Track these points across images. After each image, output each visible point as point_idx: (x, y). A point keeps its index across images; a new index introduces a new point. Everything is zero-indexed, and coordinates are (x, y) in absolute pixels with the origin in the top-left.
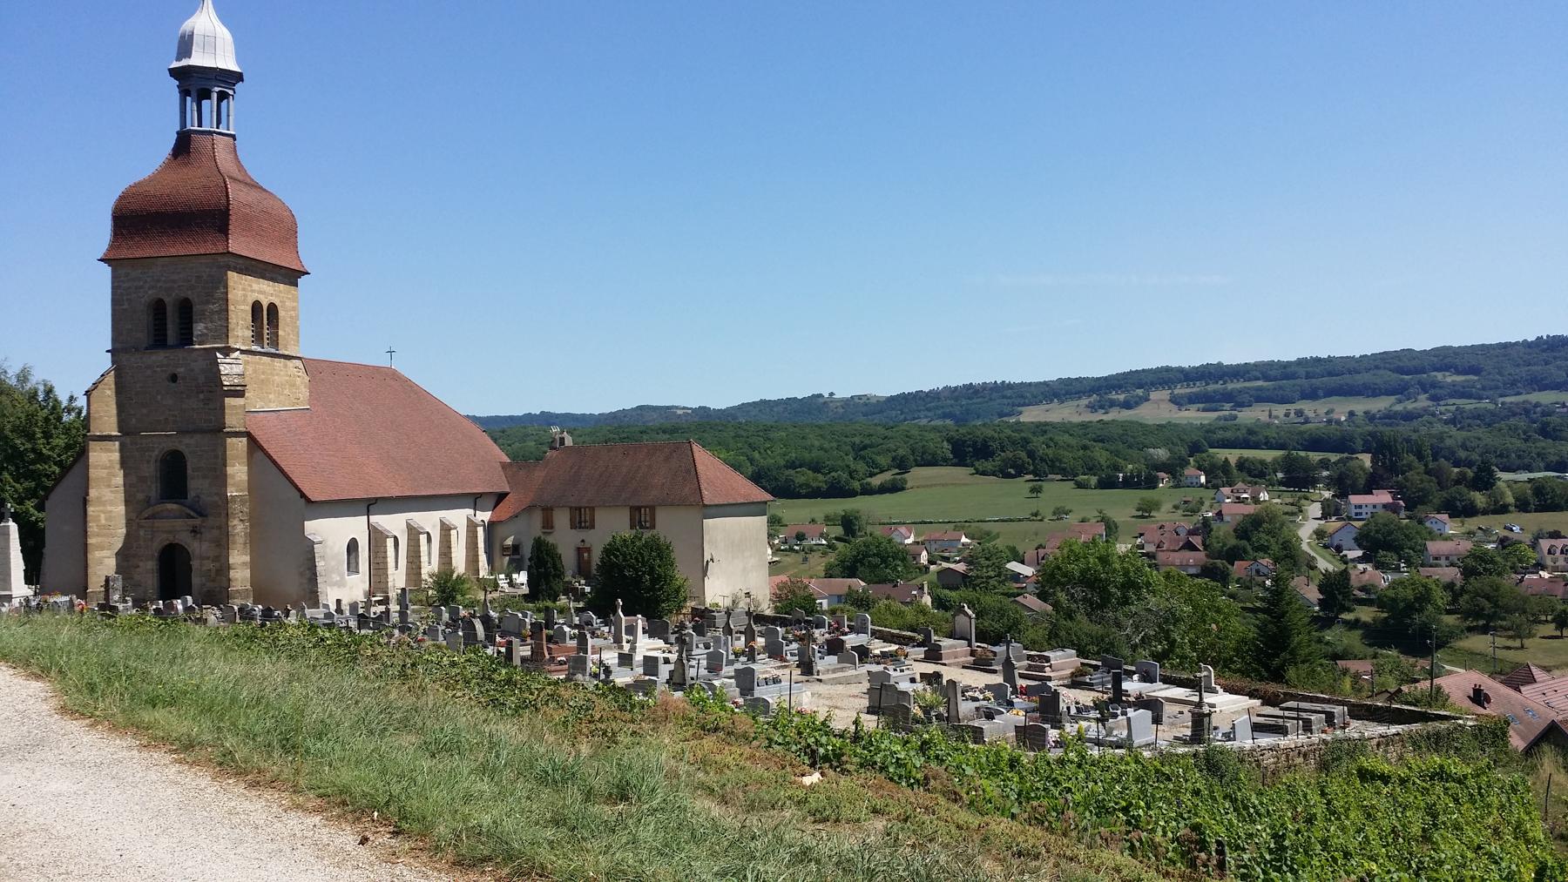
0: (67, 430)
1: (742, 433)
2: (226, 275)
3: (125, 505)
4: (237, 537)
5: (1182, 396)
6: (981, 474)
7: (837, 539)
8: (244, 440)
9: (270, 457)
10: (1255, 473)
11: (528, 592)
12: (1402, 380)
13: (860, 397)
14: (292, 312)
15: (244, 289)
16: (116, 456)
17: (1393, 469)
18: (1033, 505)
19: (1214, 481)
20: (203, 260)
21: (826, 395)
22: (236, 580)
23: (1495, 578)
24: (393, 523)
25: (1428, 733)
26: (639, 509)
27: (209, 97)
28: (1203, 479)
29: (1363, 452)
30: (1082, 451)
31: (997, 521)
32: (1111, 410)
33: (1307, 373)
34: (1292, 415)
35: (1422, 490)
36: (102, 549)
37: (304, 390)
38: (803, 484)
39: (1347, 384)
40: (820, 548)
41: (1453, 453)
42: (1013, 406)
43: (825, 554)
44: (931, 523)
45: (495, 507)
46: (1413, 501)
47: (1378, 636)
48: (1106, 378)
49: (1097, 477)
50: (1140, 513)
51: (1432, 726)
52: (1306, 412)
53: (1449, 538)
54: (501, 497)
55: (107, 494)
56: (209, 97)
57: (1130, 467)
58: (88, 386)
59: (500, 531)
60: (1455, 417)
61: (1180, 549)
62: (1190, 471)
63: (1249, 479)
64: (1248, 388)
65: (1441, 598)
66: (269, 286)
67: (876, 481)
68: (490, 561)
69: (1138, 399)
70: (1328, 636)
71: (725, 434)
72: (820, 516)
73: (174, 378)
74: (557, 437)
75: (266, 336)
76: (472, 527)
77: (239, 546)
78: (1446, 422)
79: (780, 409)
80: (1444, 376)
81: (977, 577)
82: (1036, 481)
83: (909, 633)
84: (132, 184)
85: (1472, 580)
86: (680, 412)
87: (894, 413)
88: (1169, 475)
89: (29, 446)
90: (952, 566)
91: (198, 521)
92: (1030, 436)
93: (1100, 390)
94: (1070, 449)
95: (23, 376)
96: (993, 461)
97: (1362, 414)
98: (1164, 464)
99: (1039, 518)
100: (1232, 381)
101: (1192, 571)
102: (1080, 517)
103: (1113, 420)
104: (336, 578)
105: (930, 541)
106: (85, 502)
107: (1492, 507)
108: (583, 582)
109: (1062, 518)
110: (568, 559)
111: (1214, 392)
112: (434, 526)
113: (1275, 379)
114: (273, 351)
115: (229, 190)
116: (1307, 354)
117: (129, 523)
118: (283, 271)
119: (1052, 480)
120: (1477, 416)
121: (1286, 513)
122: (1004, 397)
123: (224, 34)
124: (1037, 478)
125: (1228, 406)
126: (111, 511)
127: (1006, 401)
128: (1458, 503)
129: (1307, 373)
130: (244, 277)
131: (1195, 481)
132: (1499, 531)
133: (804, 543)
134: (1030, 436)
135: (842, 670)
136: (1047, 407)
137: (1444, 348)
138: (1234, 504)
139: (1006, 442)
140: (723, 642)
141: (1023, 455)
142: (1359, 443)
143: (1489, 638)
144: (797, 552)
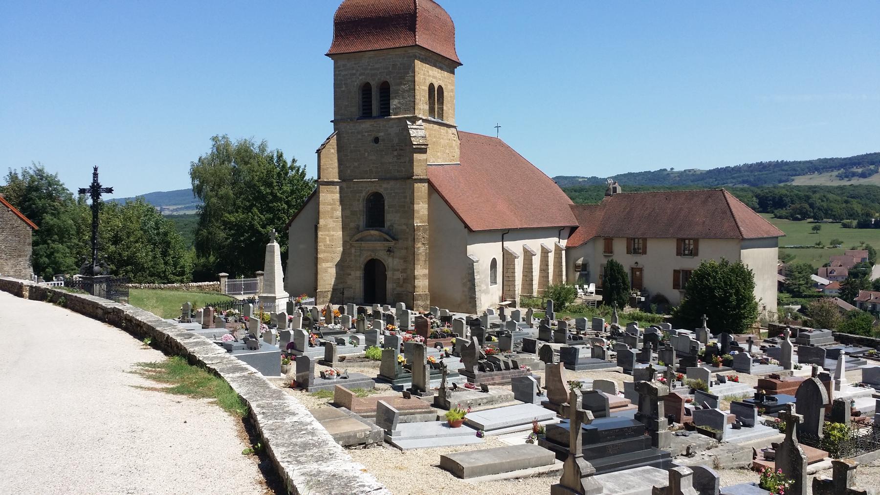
2: (414, 62)
3: (343, 232)
4: (420, 257)
6: (778, 218)
8: (426, 185)
13: (689, 171)
14: (451, 93)
15: (424, 74)
16: (337, 196)
18: (816, 238)
20: (398, 52)
21: (669, 170)
22: (419, 287)
24: (516, 247)
26: (684, 240)
31: (793, 248)
32: (853, 178)
42: (788, 176)
48: (850, 159)
49: (857, 221)
54: (573, 229)
58: (318, 146)
59: (574, 253)
66: (435, 71)
69: (870, 172)
73: (376, 140)
74: (611, 187)
77: (421, 263)
82: (816, 222)
86: (580, 180)
87: (711, 180)
89: (268, 191)
91: (392, 244)
92: (811, 194)
93: (845, 166)
94: (836, 202)
95: (263, 148)
96: (786, 209)
99: (821, 246)
102: (851, 246)
103: (860, 185)
106: (316, 228)
108: (639, 293)
109: (836, 247)
112: (538, 250)
114: (440, 121)
122: (783, 170)
124: (816, 221)
126: (333, 235)
127: (784, 173)
134: (811, 194)
136: (811, 176)
139: (795, 198)
141: (807, 206)
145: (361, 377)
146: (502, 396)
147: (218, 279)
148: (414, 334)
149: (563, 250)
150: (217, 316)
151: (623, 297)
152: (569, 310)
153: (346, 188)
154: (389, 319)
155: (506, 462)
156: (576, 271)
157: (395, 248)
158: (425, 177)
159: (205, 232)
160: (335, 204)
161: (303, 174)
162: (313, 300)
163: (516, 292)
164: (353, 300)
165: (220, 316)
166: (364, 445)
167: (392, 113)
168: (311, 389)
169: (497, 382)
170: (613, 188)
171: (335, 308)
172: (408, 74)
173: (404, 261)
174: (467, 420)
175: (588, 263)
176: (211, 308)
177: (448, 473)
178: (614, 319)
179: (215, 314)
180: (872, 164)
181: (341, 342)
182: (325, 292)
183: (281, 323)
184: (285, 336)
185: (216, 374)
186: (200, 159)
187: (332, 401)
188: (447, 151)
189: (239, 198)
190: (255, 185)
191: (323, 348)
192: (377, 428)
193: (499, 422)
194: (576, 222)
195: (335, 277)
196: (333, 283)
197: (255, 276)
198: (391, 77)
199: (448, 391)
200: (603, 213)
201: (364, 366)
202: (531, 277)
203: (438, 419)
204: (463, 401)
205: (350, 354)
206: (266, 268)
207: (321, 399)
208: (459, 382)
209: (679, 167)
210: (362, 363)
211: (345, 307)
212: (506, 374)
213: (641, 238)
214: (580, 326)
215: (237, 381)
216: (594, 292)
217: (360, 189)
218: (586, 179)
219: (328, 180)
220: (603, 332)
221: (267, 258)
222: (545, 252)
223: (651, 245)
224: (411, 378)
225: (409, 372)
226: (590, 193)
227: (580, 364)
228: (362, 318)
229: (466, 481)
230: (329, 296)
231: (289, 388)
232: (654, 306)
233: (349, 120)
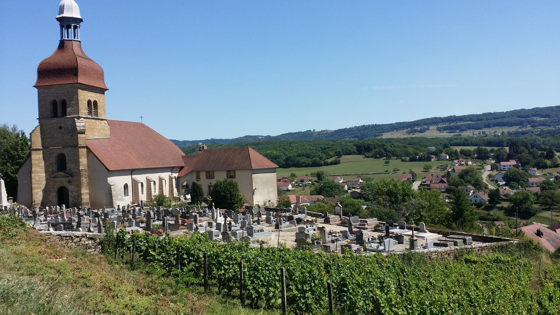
1: (281, 144)
2: (77, 91)
3: (45, 173)
4: (84, 184)
5: (441, 128)
7: (315, 181)
8: (86, 149)
9: (95, 155)
10: (467, 155)
11: (190, 202)
12: (521, 120)
13: (324, 131)
15: (84, 96)
16: (41, 156)
17: (517, 152)
18: (386, 168)
19: (452, 158)
20: (70, 86)
21: (312, 130)
22: (84, 199)
23: (552, 191)
24: (141, 178)
25: (498, 245)
27: (70, 28)
28: (448, 157)
29: (507, 146)
30: (404, 148)
33: (487, 118)
34: (481, 134)
35: (527, 159)
37: (108, 131)
38: (304, 162)
39: (501, 122)
40: (309, 185)
41: (539, 146)
43: (311, 187)
44: (349, 175)
46: (524, 164)
47: (509, 212)
48: (413, 122)
50: (425, 170)
51: (500, 243)
52: (486, 133)
53: (537, 177)
54: (182, 168)
55: (38, 169)
56: (70, 28)
57: (421, 153)
58: (31, 131)
59: (181, 180)
60: (540, 133)
61: (439, 183)
62: (443, 154)
63: (465, 157)
64: (465, 124)
65: (532, 198)
67: (329, 161)
68: (178, 191)
70: (492, 213)
71: (276, 145)
72: (309, 173)
73: (61, 128)
75: (93, 112)
76: (171, 179)
78: (537, 135)
79: (296, 135)
80: (537, 118)
81: (365, 194)
83: (320, 213)
85: (544, 191)
86: (260, 138)
88: (436, 156)
89: (16, 153)
90: (356, 190)
91: (70, 178)
95: (14, 129)
96: (372, 152)
97: (506, 133)
98: (434, 152)
99: (388, 172)
100: (459, 122)
101: (443, 190)
102: (403, 172)
104: (120, 197)
105: (348, 181)
106: (31, 172)
107: (553, 165)
109: (396, 173)
110: (205, 190)
111: (453, 126)
112: (157, 179)
113: (475, 121)
114: (96, 117)
116: (486, 111)
117: (47, 179)
118: (99, 89)
119: (393, 159)
120: (549, 132)
121: (478, 169)
122: (376, 130)
125: (458, 131)
127: (377, 131)
128: (540, 164)
129: (487, 118)
130: (84, 91)
131: (445, 158)
132: (555, 174)
133: (304, 183)
135: (290, 227)
136: (392, 133)
137: (536, 108)
138: (458, 166)
140: (249, 218)
141: (382, 150)
142: (505, 144)
143: (550, 212)
144: (301, 186)
157: (73, 180)
160: (41, 160)
180: (426, 125)
209: (318, 129)
218: (264, 137)
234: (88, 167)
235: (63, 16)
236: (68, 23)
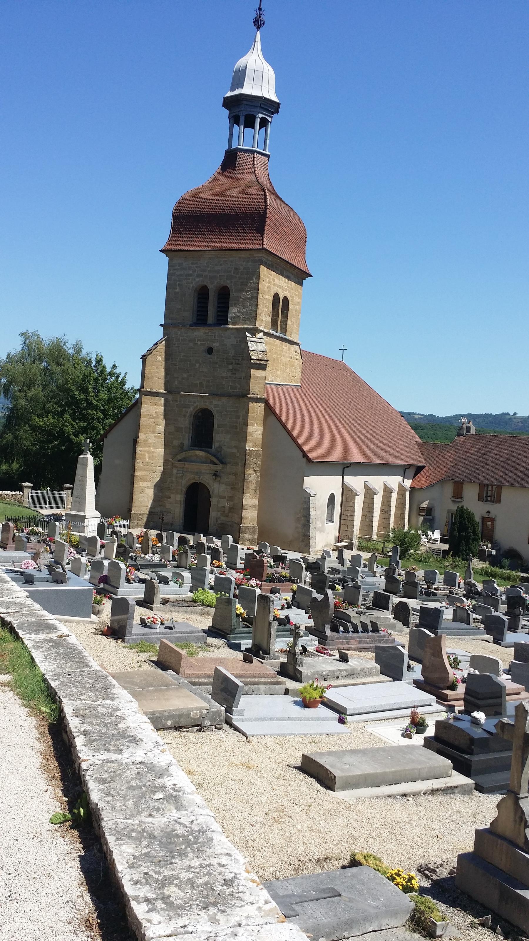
0: (109, 389)
4: (250, 484)
8: (263, 405)
9: (280, 421)
14: (297, 307)
15: (269, 282)
16: (161, 409)
20: (243, 255)
21: (512, 414)
22: (247, 518)
36: (145, 481)
45: (414, 478)
54: (419, 469)
58: (144, 352)
59: (418, 495)
66: (282, 280)
73: (210, 351)
74: (465, 426)
77: (251, 492)
84: (189, 191)
86: (416, 417)
89: (83, 396)
91: (219, 467)
106: (135, 443)
108: (489, 546)
112: (380, 488)
114: (283, 336)
115: (268, 197)
117: (166, 462)
123: (269, 72)
145: (190, 629)
146: (366, 669)
147: (21, 489)
148: (245, 575)
149: (407, 490)
150: (18, 534)
151: (473, 548)
152: (414, 559)
153: (173, 401)
154: (215, 554)
155: (390, 772)
156: (419, 515)
158: (262, 397)
159: (9, 436)
161: (123, 382)
162: (127, 523)
163: (355, 533)
164: (171, 528)
165: (20, 534)
166: (199, 727)
167: (230, 322)
168: (129, 639)
169: (353, 646)
170: (467, 427)
171: (153, 533)
172: (252, 279)
173: (231, 488)
174: (326, 699)
175: (434, 507)
176: (11, 524)
177: (313, 781)
178: (468, 573)
179: (15, 531)
181: (164, 580)
182: (140, 514)
183: (90, 548)
184: (97, 566)
185: (12, 631)
186: (8, 355)
187: (155, 659)
188: (288, 370)
189: (50, 402)
190: (69, 389)
191: (143, 586)
192: (217, 706)
193: (367, 705)
194: (424, 461)
195: (152, 498)
196: (149, 506)
197: (62, 489)
198: (231, 282)
199: (299, 657)
200: (454, 454)
201: (191, 613)
202: (371, 518)
203: (286, 692)
204: (318, 671)
205: (174, 596)
206: (77, 482)
207: (140, 654)
208: (308, 643)
210: (190, 609)
211: (164, 534)
212: (364, 637)
213: (495, 485)
214: (430, 578)
215: (42, 648)
216: (439, 540)
217: (188, 403)
218: (422, 417)
219: (152, 391)
220: (457, 588)
221: (79, 471)
222: (388, 491)
223: (506, 494)
224: (251, 635)
225: (248, 627)
226: (426, 431)
227: (443, 629)
228: (185, 551)
229: (339, 795)
230: (145, 519)
231: (101, 635)
232: (506, 562)
233: (181, 326)
234: (264, 445)
235: (242, 92)
236: (250, 111)
